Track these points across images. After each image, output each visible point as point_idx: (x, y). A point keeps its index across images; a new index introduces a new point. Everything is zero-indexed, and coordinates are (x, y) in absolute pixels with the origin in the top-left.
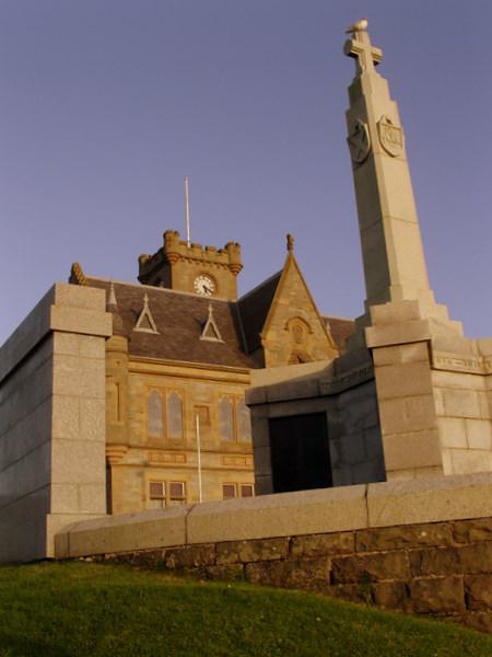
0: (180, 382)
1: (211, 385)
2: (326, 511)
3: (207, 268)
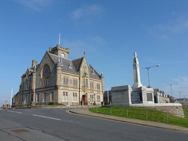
0: (68, 76)
1: (73, 76)
2: (157, 105)
3: (63, 52)
